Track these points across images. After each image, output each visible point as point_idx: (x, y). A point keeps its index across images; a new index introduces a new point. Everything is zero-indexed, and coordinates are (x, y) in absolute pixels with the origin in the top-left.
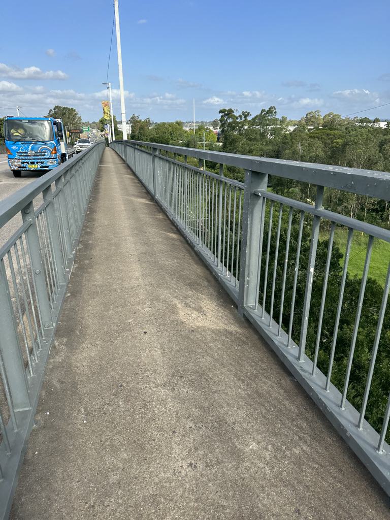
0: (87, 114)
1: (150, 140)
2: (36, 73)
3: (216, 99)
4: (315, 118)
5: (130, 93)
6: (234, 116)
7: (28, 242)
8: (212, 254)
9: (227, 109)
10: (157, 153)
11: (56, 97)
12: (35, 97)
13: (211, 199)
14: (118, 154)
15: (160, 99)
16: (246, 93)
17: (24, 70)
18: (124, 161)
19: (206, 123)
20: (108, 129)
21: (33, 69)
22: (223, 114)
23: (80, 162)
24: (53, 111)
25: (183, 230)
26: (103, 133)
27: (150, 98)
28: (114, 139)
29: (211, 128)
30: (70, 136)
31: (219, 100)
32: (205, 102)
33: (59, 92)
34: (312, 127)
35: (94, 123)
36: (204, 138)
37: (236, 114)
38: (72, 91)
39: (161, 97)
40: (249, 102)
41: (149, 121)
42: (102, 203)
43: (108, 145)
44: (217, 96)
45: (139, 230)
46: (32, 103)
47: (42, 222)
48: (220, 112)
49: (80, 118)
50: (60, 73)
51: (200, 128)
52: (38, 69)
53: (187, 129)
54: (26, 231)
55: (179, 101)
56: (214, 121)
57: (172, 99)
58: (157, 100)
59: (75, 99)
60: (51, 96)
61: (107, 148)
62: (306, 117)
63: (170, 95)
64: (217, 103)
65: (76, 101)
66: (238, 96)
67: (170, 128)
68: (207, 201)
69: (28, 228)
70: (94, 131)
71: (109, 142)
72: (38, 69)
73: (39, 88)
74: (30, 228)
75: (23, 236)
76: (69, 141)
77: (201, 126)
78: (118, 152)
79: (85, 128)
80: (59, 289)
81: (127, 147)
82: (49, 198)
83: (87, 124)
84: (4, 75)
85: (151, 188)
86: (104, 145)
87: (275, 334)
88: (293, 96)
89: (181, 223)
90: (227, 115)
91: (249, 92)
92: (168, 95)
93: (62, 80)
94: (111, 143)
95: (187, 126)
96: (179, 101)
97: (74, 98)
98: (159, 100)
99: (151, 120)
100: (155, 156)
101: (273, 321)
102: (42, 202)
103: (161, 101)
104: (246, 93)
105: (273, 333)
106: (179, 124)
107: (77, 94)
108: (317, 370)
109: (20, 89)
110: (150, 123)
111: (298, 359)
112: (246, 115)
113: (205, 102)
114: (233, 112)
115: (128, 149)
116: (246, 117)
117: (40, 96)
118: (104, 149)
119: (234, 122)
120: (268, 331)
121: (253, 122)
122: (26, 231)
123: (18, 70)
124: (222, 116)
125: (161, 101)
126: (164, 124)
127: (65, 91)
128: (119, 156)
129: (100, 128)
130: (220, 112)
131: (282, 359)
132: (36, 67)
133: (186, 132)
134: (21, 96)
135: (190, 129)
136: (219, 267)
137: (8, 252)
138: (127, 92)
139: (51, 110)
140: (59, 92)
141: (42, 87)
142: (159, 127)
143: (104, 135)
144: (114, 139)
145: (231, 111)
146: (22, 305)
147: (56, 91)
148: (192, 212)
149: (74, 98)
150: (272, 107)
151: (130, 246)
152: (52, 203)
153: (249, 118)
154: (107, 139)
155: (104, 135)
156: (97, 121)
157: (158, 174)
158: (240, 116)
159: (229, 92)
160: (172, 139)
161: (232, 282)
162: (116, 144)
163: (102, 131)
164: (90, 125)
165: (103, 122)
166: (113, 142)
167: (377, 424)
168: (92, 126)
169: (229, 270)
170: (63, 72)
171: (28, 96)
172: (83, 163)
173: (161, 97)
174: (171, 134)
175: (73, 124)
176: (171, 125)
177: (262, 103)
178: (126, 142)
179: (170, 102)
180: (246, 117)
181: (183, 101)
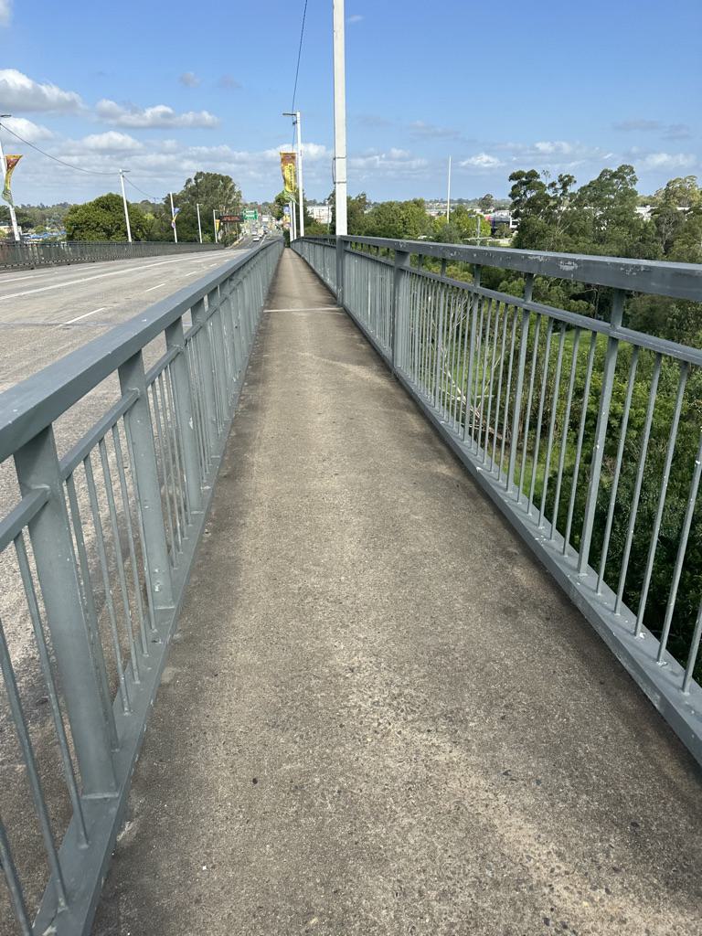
0: (254, 188)
1: (382, 236)
2: (165, 115)
3: (485, 158)
4: (685, 191)
5: (327, 150)
6: (541, 184)
7: (130, 436)
8: (480, 448)
9: (526, 172)
10: (407, 264)
11: (198, 158)
12: (163, 159)
13: (506, 364)
14: (311, 268)
15: (381, 159)
16: (542, 146)
17: (144, 112)
18: (333, 298)
19: (468, 202)
20: (289, 212)
21: (161, 109)
22: (516, 182)
23: (241, 272)
24: (193, 181)
25: (430, 409)
26: (281, 222)
27: (364, 157)
28: (302, 234)
29: (478, 211)
30: (221, 227)
31: (491, 159)
32: (464, 164)
33: (204, 149)
34: (687, 209)
35: (266, 204)
36: (478, 230)
37: (544, 180)
38: (226, 148)
39: (383, 156)
40: (569, 159)
41: (365, 198)
42: (275, 392)
43: (288, 244)
44: (487, 153)
45: (385, 530)
46: (159, 170)
47: (160, 395)
48: (513, 177)
49: (239, 194)
50: (206, 116)
51: (459, 212)
52: (169, 110)
53: (433, 213)
54: (126, 413)
55: (415, 163)
56: (484, 199)
57: (401, 159)
58: (376, 160)
59: (230, 162)
60: (191, 158)
61: (287, 252)
62: (667, 190)
63: (400, 151)
64: (486, 165)
65: (234, 166)
66: (528, 152)
67: (402, 212)
68: (494, 367)
69: (132, 406)
70: (265, 219)
71: (292, 240)
72: (169, 110)
73: (170, 143)
74: (136, 406)
75: (120, 422)
76: (220, 238)
77: (460, 208)
78: (312, 264)
79: (249, 214)
80: (190, 525)
81: (348, 258)
82: (199, 317)
83: (254, 206)
84: (112, 122)
85: (386, 349)
86: (281, 245)
87: (650, 657)
88: (635, 150)
89: (427, 397)
90: (524, 183)
91: (549, 143)
92: (396, 152)
93: (209, 127)
94: (294, 241)
95: (431, 208)
96: (415, 163)
97: (229, 159)
98: (378, 162)
99: (367, 197)
100: (402, 271)
101: (556, 533)
102: (163, 351)
103: (382, 162)
104: (542, 146)
105: (646, 654)
106: (418, 203)
107: (235, 153)
108: (602, 584)
109: (139, 145)
110: (366, 203)
111: (578, 570)
112: (566, 181)
113: (464, 164)
114: (538, 177)
115: (352, 265)
116: (564, 186)
117: (172, 157)
118: (283, 252)
119: (539, 196)
120: (612, 621)
121: (579, 200)
122: (126, 413)
123: (134, 111)
124: (514, 187)
125: (382, 162)
126: (391, 204)
127: (214, 149)
128: (314, 272)
129: (276, 213)
130: (513, 177)
131: (457, 453)
132: (166, 105)
133: (432, 218)
134: (140, 158)
135: (439, 214)
136: (509, 492)
137: (84, 460)
138: (324, 147)
139: (189, 181)
140: (204, 149)
141: (174, 141)
142: (383, 209)
143: (282, 226)
144: (302, 234)
145: (533, 174)
146: (124, 542)
147: (198, 148)
148: (458, 386)
149: (229, 159)
150: (627, 167)
151: (334, 483)
152: (219, 310)
153: (572, 189)
154: (287, 234)
155: (282, 226)
156: (272, 200)
157: (364, 284)
158: (553, 185)
159: (511, 145)
160: (406, 232)
161: (500, 481)
162: (306, 246)
163: (278, 219)
164: (259, 207)
165: (281, 202)
166: (299, 239)
167: (679, 650)
168: (261, 209)
169: (590, 562)
170: (210, 114)
171: (152, 159)
172: (249, 272)
173: (383, 156)
174: (404, 223)
175: (228, 206)
176: (403, 206)
177: (573, 164)
178: (344, 241)
179: (398, 164)
180: (564, 186)
181: (423, 162)
